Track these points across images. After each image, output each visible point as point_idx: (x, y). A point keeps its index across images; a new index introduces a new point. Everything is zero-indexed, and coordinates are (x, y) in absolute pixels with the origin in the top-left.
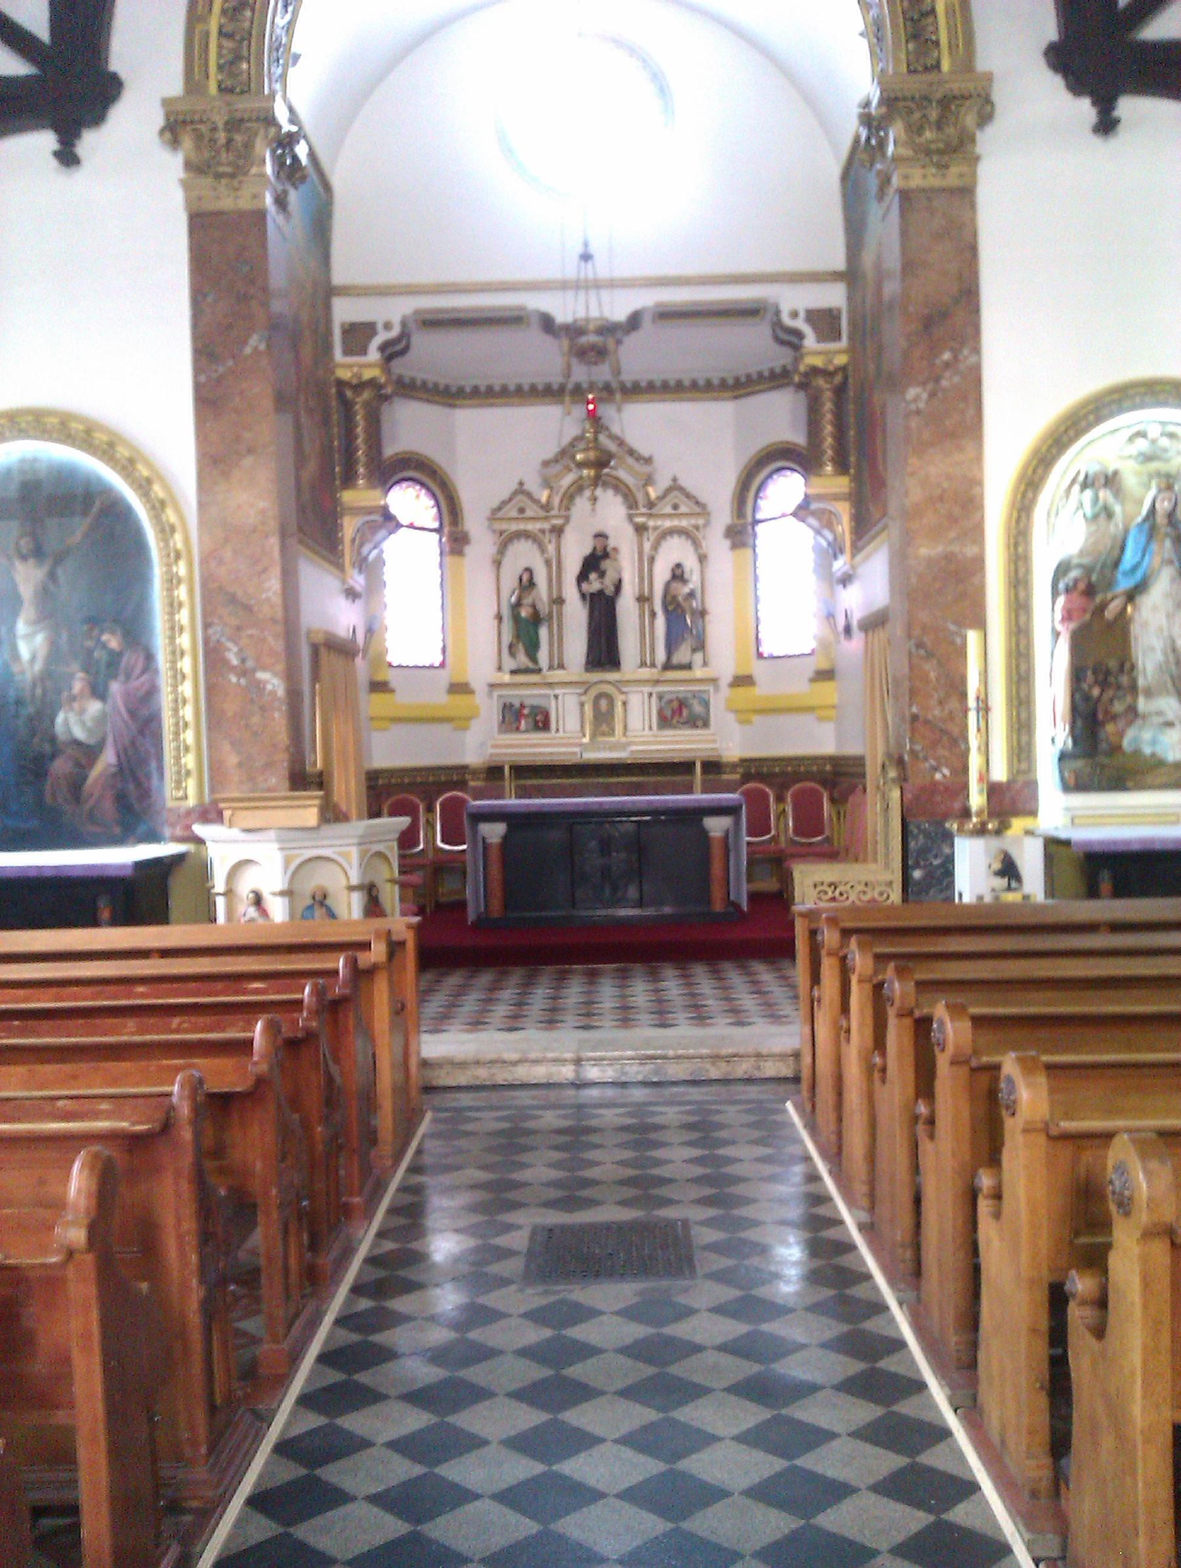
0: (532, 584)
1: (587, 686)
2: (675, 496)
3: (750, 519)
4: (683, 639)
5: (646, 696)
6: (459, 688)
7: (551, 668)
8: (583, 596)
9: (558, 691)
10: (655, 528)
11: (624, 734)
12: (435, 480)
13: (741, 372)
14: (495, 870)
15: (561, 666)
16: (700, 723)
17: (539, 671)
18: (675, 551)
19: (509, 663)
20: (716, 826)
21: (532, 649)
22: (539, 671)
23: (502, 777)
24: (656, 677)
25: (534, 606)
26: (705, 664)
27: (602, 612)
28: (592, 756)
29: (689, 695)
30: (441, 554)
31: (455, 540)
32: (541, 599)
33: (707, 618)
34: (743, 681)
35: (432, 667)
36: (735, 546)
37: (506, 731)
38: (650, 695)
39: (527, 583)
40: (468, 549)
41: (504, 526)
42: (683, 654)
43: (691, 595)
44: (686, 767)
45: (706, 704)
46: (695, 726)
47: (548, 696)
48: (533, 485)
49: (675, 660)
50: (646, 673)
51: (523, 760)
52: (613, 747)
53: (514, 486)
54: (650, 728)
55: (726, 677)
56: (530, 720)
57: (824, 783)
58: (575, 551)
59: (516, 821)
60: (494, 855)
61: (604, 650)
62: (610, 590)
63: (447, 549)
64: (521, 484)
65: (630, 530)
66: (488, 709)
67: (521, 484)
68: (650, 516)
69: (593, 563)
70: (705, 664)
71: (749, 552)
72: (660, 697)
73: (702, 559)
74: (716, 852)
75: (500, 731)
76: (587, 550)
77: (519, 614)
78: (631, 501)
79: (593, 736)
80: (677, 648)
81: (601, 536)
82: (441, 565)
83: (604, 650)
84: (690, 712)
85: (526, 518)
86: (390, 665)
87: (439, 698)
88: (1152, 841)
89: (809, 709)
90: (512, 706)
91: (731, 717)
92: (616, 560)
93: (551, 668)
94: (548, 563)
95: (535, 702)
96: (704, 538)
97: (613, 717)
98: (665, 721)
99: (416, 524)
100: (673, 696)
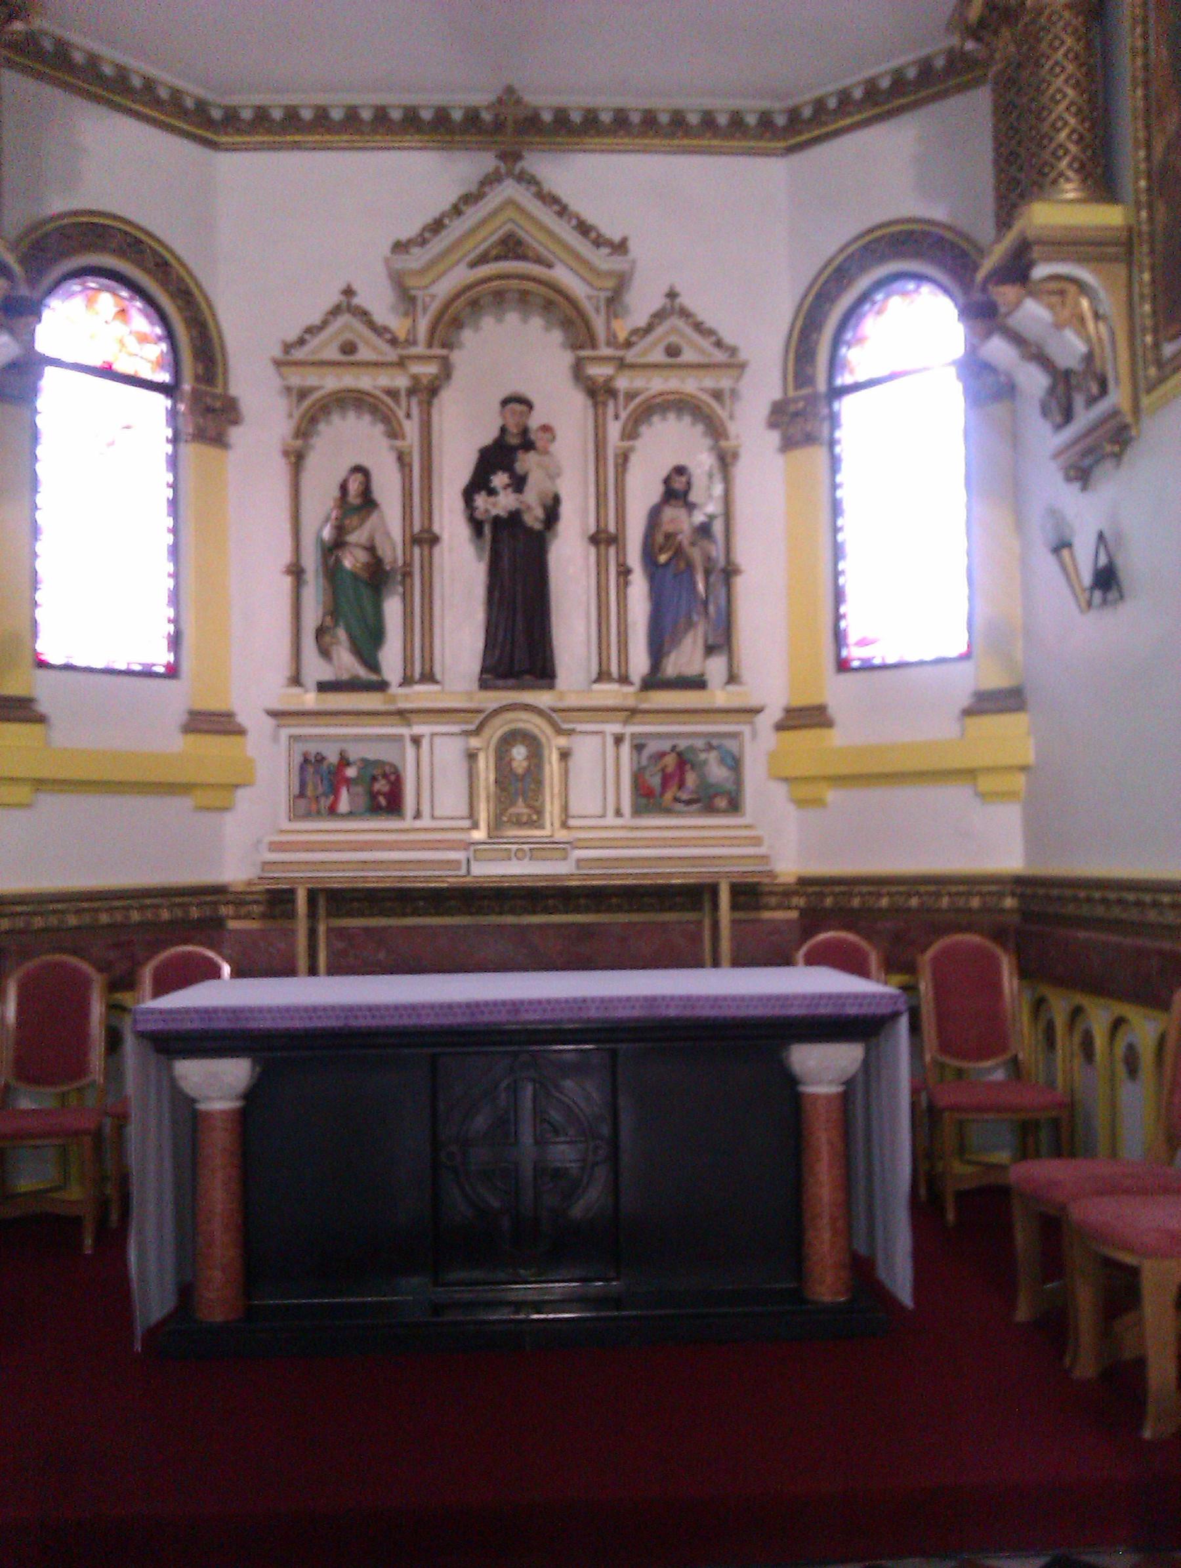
0: (368, 503)
1: (480, 720)
2: (673, 329)
3: (822, 387)
4: (690, 625)
5: (610, 741)
6: (210, 723)
7: (407, 681)
8: (477, 526)
9: (417, 730)
10: (631, 396)
11: (564, 825)
12: (164, 283)
13: (804, 98)
14: (219, 1194)
15: (428, 677)
16: (722, 803)
17: (381, 686)
18: (671, 443)
19: (316, 669)
20: (822, 1067)
21: (368, 642)
22: (381, 686)
23: (291, 915)
24: (631, 702)
25: (371, 549)
26: (732, 678)
27: (517, 561)
28: (491, 870)
29: (700, 743)
30: (175, 440)
31: (203, 403)
32: (387, 534)
33: (741, 584)
34: (806, 717)
35: (147, 673)
36: (788, 445)
37: (308, 815)
38: (619, 739)
39: (358, 501)
40: (235, 434)
41: (310, 378)
42: (686, 657)
43: (704, 530)
44: (695, 895)
45: (735, 764)
46: (710, 809)
47: (399, 738)
48: (378, 300)
49: (672, 667)
50: (610, 694)
51: (339, 878)
52: (539, 850)
53: (333, 297)
54: (618, 813)
55: (775, 704)
56: (359, 789)
57: (999, 935)
59: (280, 1051)
60: (219, 1146)
61: (520, 647)
62: (534, 518)
63: (188, 429)
64: (349, 292)
65: (578, 400)
66: (269, 760)
67: (349, 292)
68: (622, 365)
69: (500, 458)
70: (732, 678)
71: (819, 454)
72: (638, 748)
73: (726, 461)
74: (823, 1140)
75: (294, 816)
76: (487, 436)
77: (338, 561)
78: (576, 327)
79: (496, 825)
80: (676, 641)
81: (517, 402)
82: (173, 463)
83: (520, 647)
84: (702, 778)
85: (367, 370)
86: (42, 664)
87: (162, 739)
88: (387, 819)
89: (969, 774)
90: (320, 759)
91: (780, 791)
92: (546, 452)
93: (407, 681)
94: (402, 460)
95: (373, 753)
96: (731, 417)
97: (539, 783)
98: (647, 798)
99: (121, 367)
100: (666, 745)
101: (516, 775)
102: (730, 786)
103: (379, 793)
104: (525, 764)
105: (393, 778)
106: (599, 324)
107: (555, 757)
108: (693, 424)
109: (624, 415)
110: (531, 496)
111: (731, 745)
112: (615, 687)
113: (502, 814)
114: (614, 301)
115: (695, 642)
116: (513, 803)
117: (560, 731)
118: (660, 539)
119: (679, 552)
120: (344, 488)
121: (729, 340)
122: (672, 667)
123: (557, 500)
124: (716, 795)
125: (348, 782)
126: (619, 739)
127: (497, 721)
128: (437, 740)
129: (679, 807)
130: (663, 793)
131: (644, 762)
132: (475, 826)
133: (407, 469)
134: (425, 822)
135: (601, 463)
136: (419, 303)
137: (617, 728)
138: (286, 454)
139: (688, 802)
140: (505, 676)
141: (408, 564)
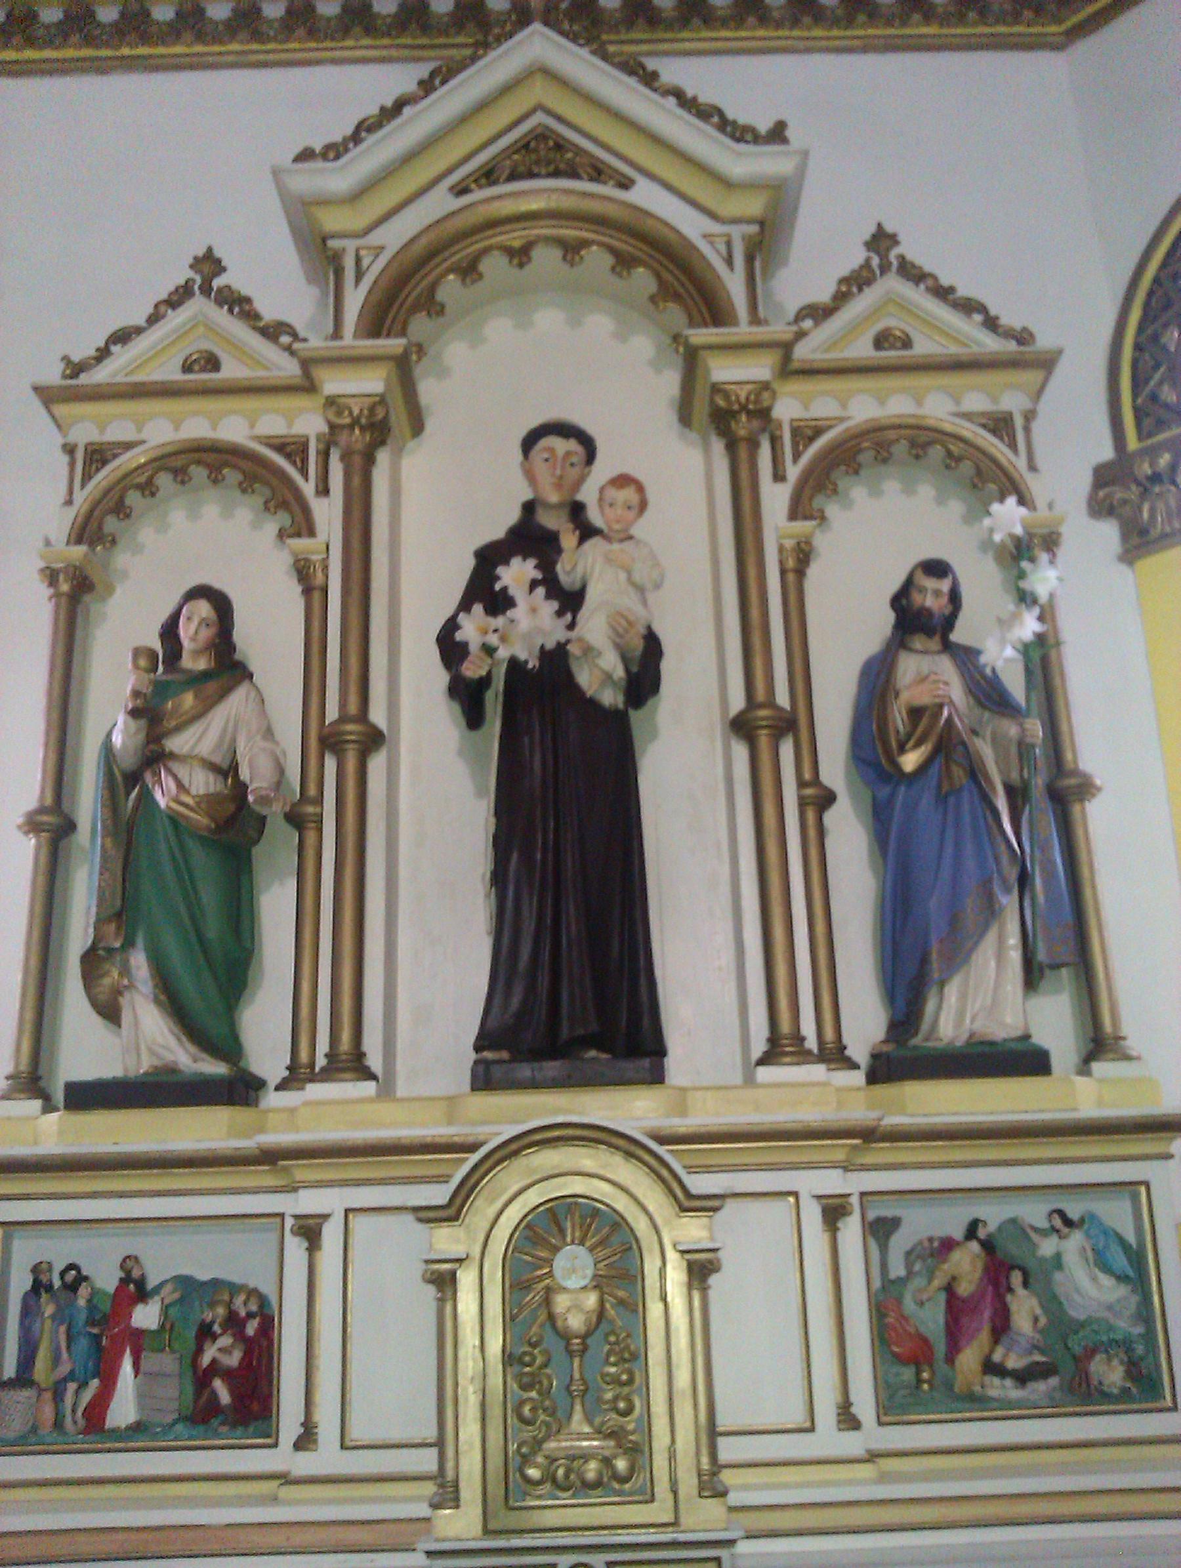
0: (228, 667)
5: (812, 1215)
8: (468, 697)
10: (805, 434)
15: (354, 1064)
17: (241, 1090)
21: (209, 991)
22: (241, 1090)
25: (228, 770)
27: (563, 768)
29: (1035, 1213)
33: (1099, 819)
39: (201, 660)
42: (984, 994)
45: (1135, 1267)
46: (1084, 1394)
48: (277, 281)
49: (952, 1017)
54: (848, 1420)
56: (165, 1362)
58: (441, 507)
61: (575, 988)
62: (599, 675)
68: (788, 370)
70: (1099, 1044)
72: (880, 1230)
77: (146, 797)
78: (683, 286)
80: (958, 955)
83: (575, 988)
84: (1052, 1303)
90: (75, 1278)
95: (204, 1259)
96: (1032, 467)
97: (632, 1356)
101: (565, 1336)
102: (1125, 1326)
103: (215, 1368)
104: (591, 1300)
105: (251, 1328)
106: (734, 284)
107: (676, 1276)
108: (940, 500)
109: (793, 472)
110: (594, 626)
111: (1117, 1214)
112: (818, 1071)
113: (526, 1460)
114: (765, 243)
115: (1000, 956)
116: (559, 1426)
117: (690, 1203)
118: (898, 719)
119: (948, 746)
120: (169, 633)
121: (1009, 318)
122: (952, 1017)
123: (653, 645)
124: (1091, 1352)
125: (138, 1340)
126: (834, 1212)
127: (510, 1177)
128: (359, 1223)
129: (999, 1388)
130: (954, 1348)
131: (897, 1270)
132: (448, 1494)
133: (317, 596)
134: (326, 1458)
135: (778, 447)
136: (349, 263)
137: (832, 1182)
138: (51, 576)
139: (1022, 1377)
140: (537, 1055)
141: (310, 797)
